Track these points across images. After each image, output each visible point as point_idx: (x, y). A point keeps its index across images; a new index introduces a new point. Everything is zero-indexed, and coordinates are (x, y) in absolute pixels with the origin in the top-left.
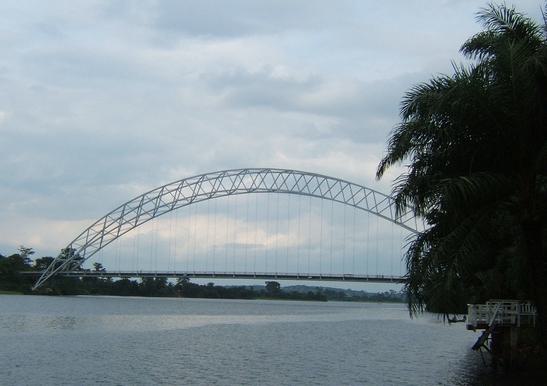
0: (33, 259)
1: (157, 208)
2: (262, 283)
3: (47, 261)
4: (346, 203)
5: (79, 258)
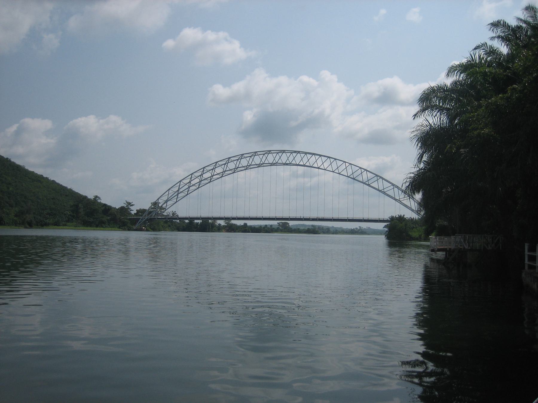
0: (134, 210)
1: (201, 181)
2: (275, 223)
3: (143, 211)
4: (333, 172)
5: (161, 208)
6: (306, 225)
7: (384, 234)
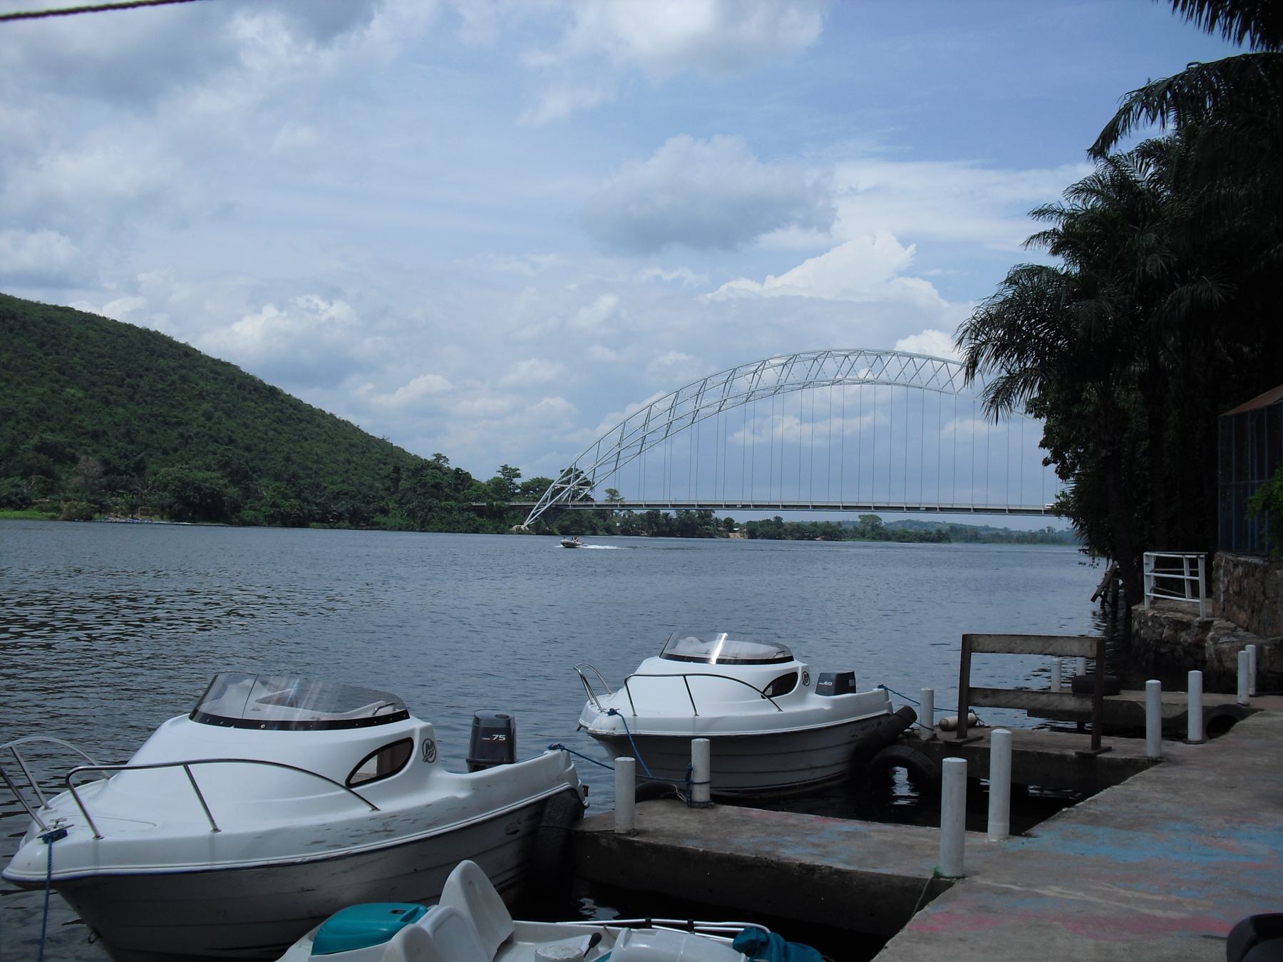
2: (854, 517)
6: (922, 522)
7: (1072, 543)
